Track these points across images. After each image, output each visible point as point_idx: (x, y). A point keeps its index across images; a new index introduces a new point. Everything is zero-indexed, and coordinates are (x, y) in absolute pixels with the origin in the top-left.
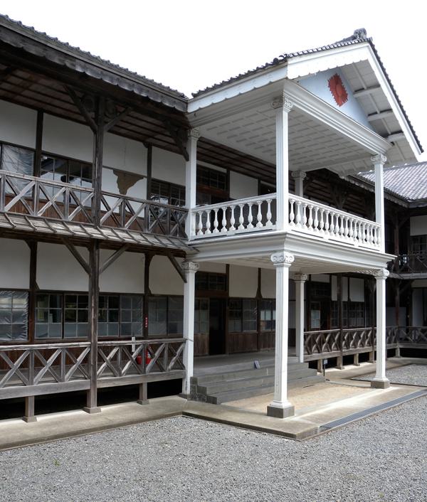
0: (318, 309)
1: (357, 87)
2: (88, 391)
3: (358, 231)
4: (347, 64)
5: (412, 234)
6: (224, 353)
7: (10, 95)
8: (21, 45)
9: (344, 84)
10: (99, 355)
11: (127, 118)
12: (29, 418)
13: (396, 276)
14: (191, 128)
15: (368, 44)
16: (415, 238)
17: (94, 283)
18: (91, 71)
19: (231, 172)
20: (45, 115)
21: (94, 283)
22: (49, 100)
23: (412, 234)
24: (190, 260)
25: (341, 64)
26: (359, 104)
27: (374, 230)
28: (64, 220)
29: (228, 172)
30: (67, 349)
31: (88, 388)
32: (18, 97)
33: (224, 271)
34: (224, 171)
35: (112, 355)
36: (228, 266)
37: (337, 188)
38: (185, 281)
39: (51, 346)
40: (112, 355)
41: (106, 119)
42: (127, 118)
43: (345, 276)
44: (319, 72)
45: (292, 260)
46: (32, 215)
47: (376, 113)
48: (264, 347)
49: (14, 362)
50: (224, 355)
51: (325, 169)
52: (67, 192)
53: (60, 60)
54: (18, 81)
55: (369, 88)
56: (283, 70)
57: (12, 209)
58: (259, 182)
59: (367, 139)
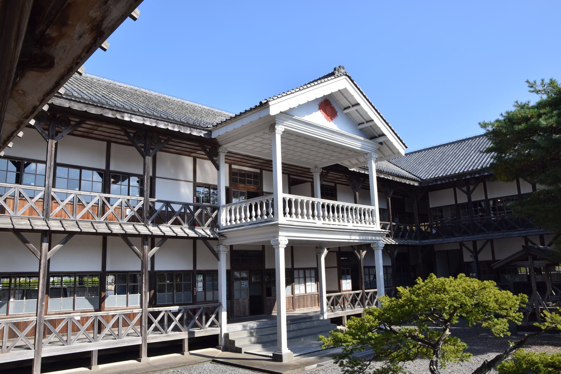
0: (348, 274)
1: (346, 106)
2: (141, 345)
3: (352, 216)
4: (333, 91)
5: (431, 207)
6: (263, 314)
7: (86, 134)
8: (85, 109)
9: (334, 105)
10: (149, 319)
11: (166, 146)
12: (93, 367)
13: (402, 242)
14: (220, 146)
15: (344, 77)
16: (435, 209)
17: (469, 198)
18: (136, 119)
19: (264, 171)
20: (112, 144)
21: (469, 198)
22: (113, 135)
23: (431, 207)
24: (221, 244)
25: (327, 93)
26: (350, 119)
27: (364, 213)
28: (121, 222)
29: (261, 172)
30: (125, 315)
31: (140, 343)
32: (91, 135)
33: (261, 249)
34: (258, 171)
35: (159, 318)
36: (263, 246)
37: (339, 180)
38: (219, 260)
39: (160, 309)
40: (159, 318)
41: (152, 147)
42: (166, 146)
43: (201, 274)
44: (281, 112)
45: (287, 242)
46: (97, 220)
47: (364, 123)
48: (299, 307)
49: (176, 325)
50: (263, 315)
51: (337, 165)
52: (123, 203)
53: (113, 115)
54: (89, 126)
55: (353, 106)
56: (265, 110)
57: (83, 217)
58: (289, 177)
59: (356, 142)
